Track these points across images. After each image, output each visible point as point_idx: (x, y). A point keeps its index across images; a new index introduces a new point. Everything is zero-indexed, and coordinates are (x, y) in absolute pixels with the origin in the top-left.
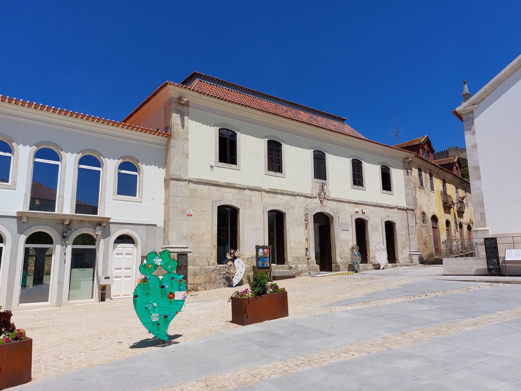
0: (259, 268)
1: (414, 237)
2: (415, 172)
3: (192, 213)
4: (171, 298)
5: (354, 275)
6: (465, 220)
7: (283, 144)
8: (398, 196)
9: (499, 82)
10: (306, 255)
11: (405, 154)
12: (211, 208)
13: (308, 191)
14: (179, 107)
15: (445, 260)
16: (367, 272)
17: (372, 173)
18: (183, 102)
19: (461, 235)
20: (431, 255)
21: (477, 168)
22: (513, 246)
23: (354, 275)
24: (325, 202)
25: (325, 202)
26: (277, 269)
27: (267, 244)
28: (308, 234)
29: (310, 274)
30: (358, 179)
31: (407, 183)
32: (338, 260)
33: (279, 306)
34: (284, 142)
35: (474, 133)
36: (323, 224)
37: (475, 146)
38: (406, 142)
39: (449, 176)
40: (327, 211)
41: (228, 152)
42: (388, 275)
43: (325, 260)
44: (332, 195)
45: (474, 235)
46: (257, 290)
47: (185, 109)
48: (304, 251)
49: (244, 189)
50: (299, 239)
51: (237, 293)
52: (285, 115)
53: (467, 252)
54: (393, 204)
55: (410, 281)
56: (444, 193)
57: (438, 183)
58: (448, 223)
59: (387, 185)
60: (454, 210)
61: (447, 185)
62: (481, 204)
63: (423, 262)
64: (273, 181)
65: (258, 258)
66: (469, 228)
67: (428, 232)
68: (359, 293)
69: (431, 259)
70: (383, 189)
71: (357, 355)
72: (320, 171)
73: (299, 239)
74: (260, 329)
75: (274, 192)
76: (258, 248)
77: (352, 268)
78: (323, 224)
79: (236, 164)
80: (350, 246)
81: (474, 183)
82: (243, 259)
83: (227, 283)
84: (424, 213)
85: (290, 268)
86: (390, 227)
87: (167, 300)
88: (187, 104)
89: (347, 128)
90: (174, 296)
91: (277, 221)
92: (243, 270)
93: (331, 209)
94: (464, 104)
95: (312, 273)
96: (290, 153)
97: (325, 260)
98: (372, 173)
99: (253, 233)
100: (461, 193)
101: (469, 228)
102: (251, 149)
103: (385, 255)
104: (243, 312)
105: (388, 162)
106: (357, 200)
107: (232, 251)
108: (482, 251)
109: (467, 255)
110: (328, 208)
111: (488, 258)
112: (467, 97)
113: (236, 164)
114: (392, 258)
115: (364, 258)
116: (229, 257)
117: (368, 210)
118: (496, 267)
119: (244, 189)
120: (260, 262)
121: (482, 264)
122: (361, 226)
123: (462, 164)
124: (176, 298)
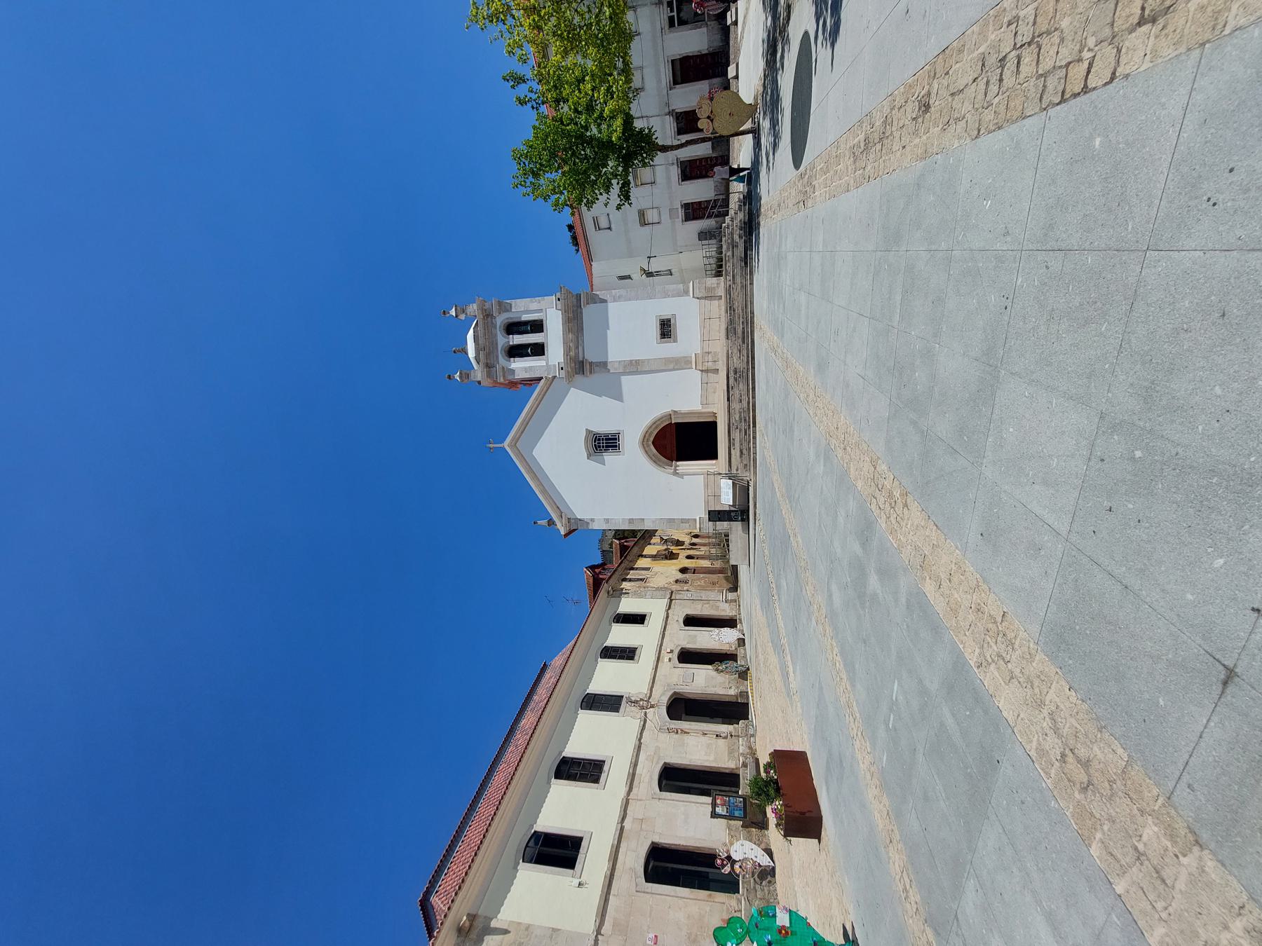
0: (745, 816)
1: (704, 595)
2: (625, 585)
3: (651, 935)
4: (787, 933)
5: (753, 671)
6: (687, 540)
7: (564, 754)
8: (654, 607)
9: (544, 491)
10: (726, 738)
11: (602, 594)
12: (648, 896)
13: (636, 724)
14: (473, 935)
15: (733, 562)
16: (749, 655)
17: (620, 635)
18: (467, 924)
19: (704, 545)
20: (727, 579)
21: (631, 521)
22: (717, 496)
23: (753, 672)
24: (652, 701)
25: (652, 701)
26: (746, 777)
27: (708, 800)
28: (696, 732)
29: (753, 736)
30: (627, 654)
31: (638, 595)
32: (732, 692)
33: (791, 764)
34: (561, 753)
35: (592, 520)
36: (685, 708)
37: (607, 521)
38: (586, 593)
39: (635, 550)
40: (665, 700)
41: (558, 851)
42: (751, 631)
43: (731, 711)
44: (645, 690)
45: (705, 531)
46: (772, 792)
47: (479, 924)
48: (721, 741)
49: (622, 829)
50: (702, 746)
51: (778, 825)
52: (521, 749)
53: (723, 542)
54: (663, 614)
55: (757, 601)
56: (654, 557)
57: (641, 563)
58: (689, 557)
59: (638, 619)
60: (674, 549)
61: (494, 924)
62: (671, 521)
63: (735, 588)
64: (615, 776)
65: (730, 817)
66: (696, 536)
67: (699, 579)
68: (774, 660)
69: (732, 579)
70: (596, 781)
71: (836, 650)
72: (610, 703)
73: (702, 746)
74: (824, 788)
75: (632, 776)
76: (714, 815)
77: (744, 674)
78: (685, 708)
79: (581, 839)
80: (715, 673)
81: (648, 526)
82: (732, 844)
83: (769, 878)
84: (677, 581)
85: (744, 765)
86: (691, 621)
87: (790, 939)
88: (472, 917)
89: (558, 661)
90: (783, 927)
91: (676, 778)
92: (748, 844)
93: (663, 694)
94: (559, 526)
95: (751, 731)
96: (576, 748)
97: (731, 711)
98: (620, 635)
99: (693, 823)
100: (655, 540)
101: (696, 536)
102: (562, 809)
103: (726, 631)
104: (805, 823)
105: (609, 614)
106: (653, 658)
107: (719, 862)
108: (723, 526)
109: (727, 541)
110: (662, 697)
111: (730, 520)
112: (551, 522)
113: (581, 839)
114: (731, 623)
115: (732, 657)
116: (727, 869)
117: (668, 645)
118: (741, 513)
119: (622, 829)
120: (737, 813)
121: (737, 526)
122: (688, 656)
123: (621, 535)
124: (788, 925)
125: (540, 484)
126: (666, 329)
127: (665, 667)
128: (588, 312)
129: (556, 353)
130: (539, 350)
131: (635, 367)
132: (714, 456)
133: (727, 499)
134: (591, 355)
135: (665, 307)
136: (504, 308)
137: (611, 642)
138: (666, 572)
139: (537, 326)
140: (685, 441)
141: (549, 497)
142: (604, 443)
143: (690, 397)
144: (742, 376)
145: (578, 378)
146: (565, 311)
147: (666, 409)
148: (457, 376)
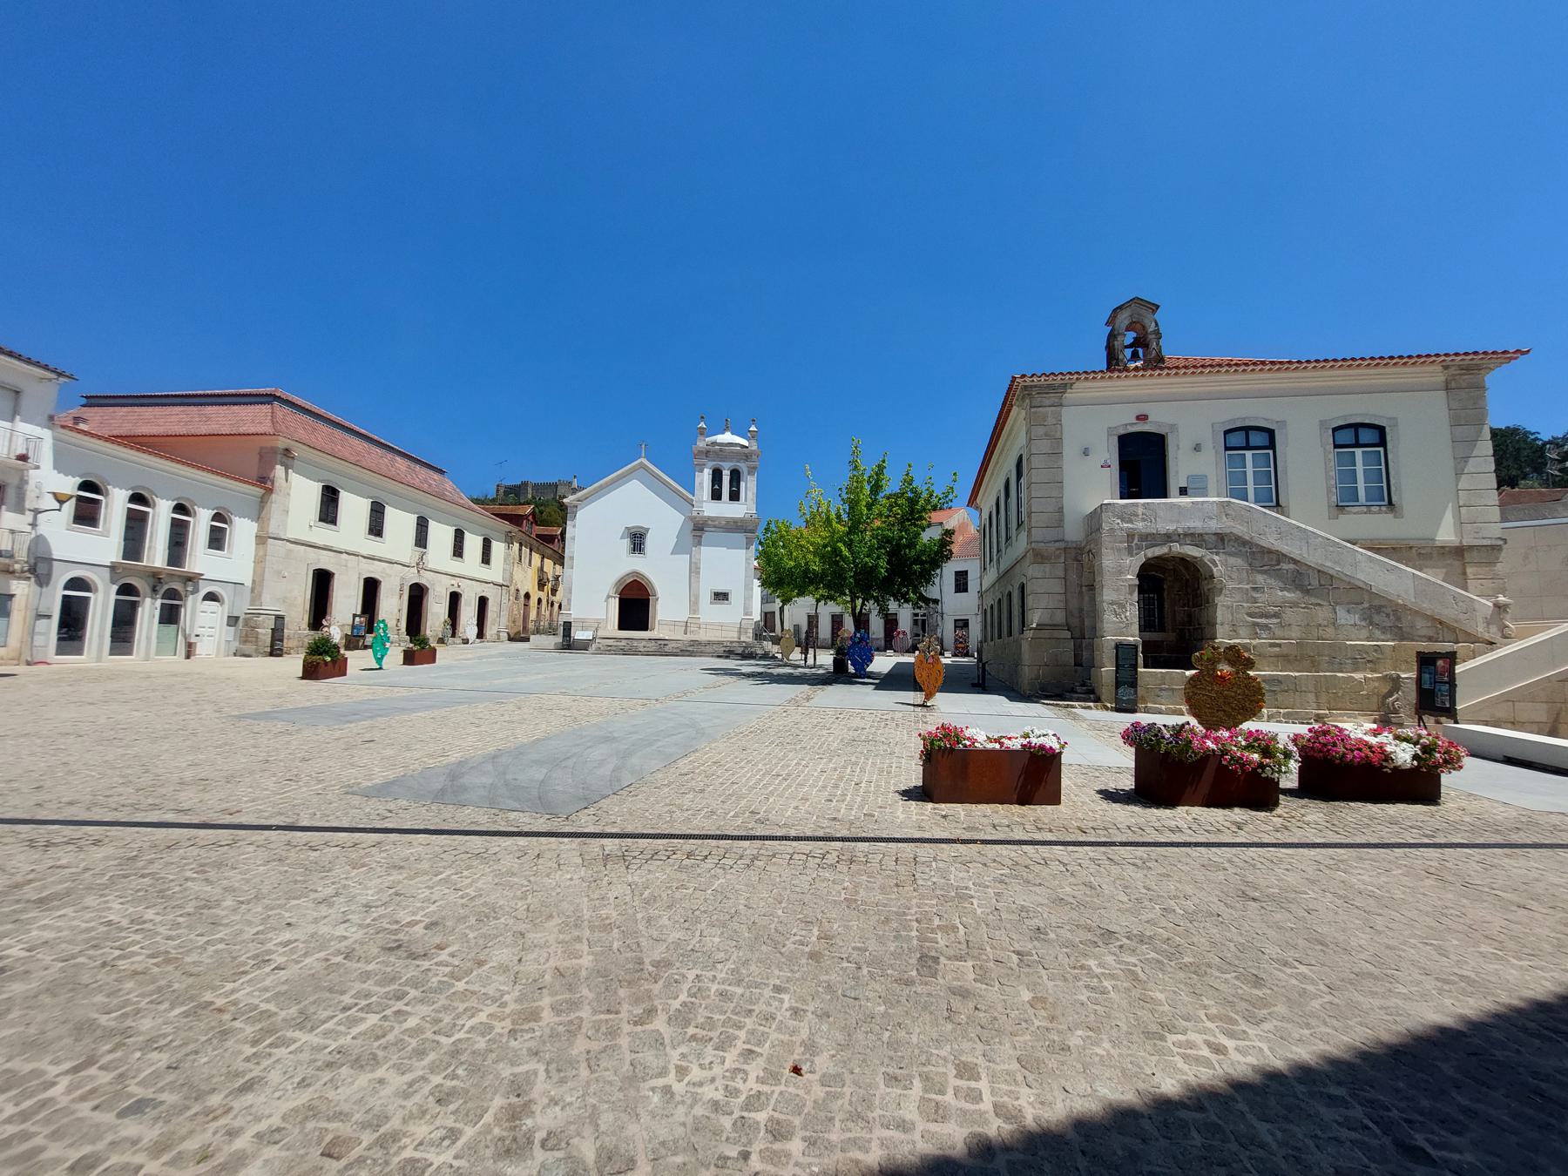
6: (556, 599)
8: (495, 572)
9: (601, 487)
13: (406, 560)
17: (473, 543)
21: (572, 558)
22: (583, 629)
30: (458, 551)
40: (423, 581)
44: (430, 566)
53: (551, 631)
56: (541, 569)
57: (536, 558)
58: (540, 601)
59: (486, 559)
63: (511, 639)
65: (353, 627)
72: (421, 540)
76: (355, 616)
86: (483, 602)
89: (448, 485)
98: (473, 543)
102: (354, 508)
103: (475, 630)
105: (490, 534)
106: (454, 572)
110: (425, 579)
112: (574, 491)
114: (480, 635)
117: (464, 583)
118: (569, 644)
121: (559, 639)
122: (455, 598)
125: (608, 485)
126: (721, 596)
127: (448, 581)
128: (741, 537)
129: (712, 509)
130: (716, 495)
131: (694, 570)
132: (621, 627)
133: (579, 635)
134: (706, 536)
135: (736, 598)
136: (751, 470)
137: (467, 535)
138: (526, 580)
139: (735, 496)
140: (635, 606)
141: (596, 491)
142: (637, 541)
143: (667, 612)
144: (662, 649)
145: (691, 526)
146: (741, 520)
147: (659, 594)
148: (702, 425)
